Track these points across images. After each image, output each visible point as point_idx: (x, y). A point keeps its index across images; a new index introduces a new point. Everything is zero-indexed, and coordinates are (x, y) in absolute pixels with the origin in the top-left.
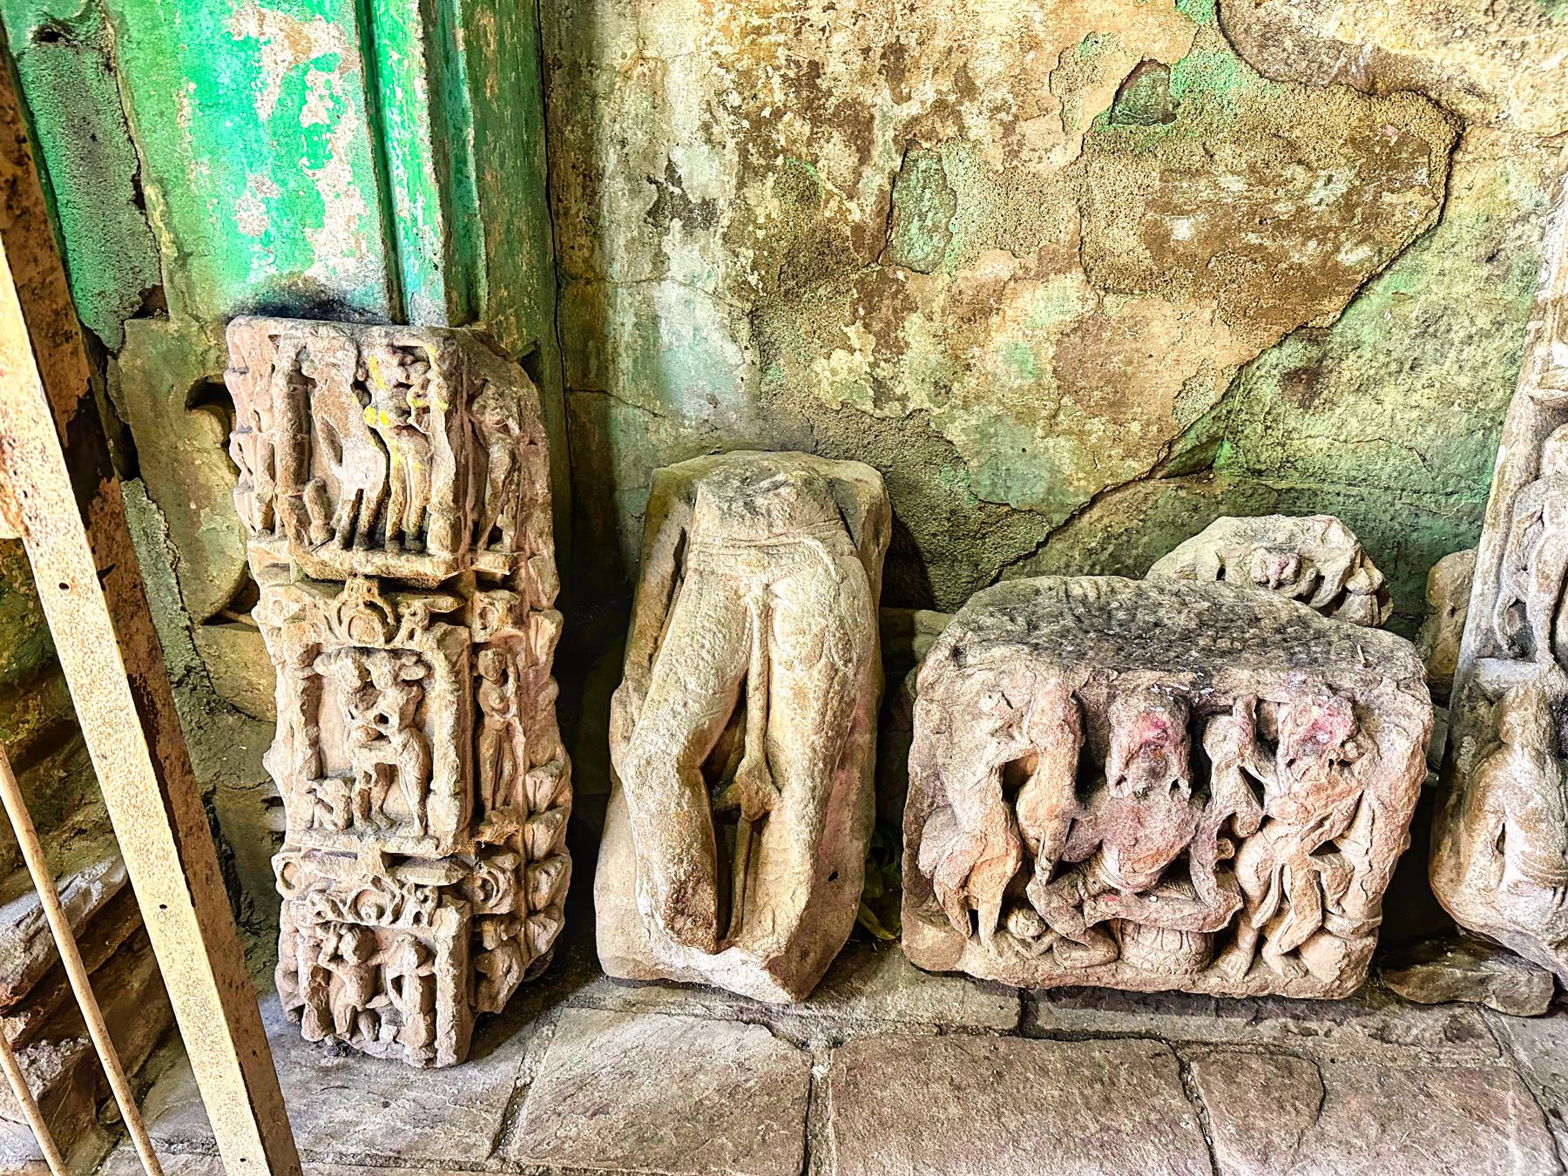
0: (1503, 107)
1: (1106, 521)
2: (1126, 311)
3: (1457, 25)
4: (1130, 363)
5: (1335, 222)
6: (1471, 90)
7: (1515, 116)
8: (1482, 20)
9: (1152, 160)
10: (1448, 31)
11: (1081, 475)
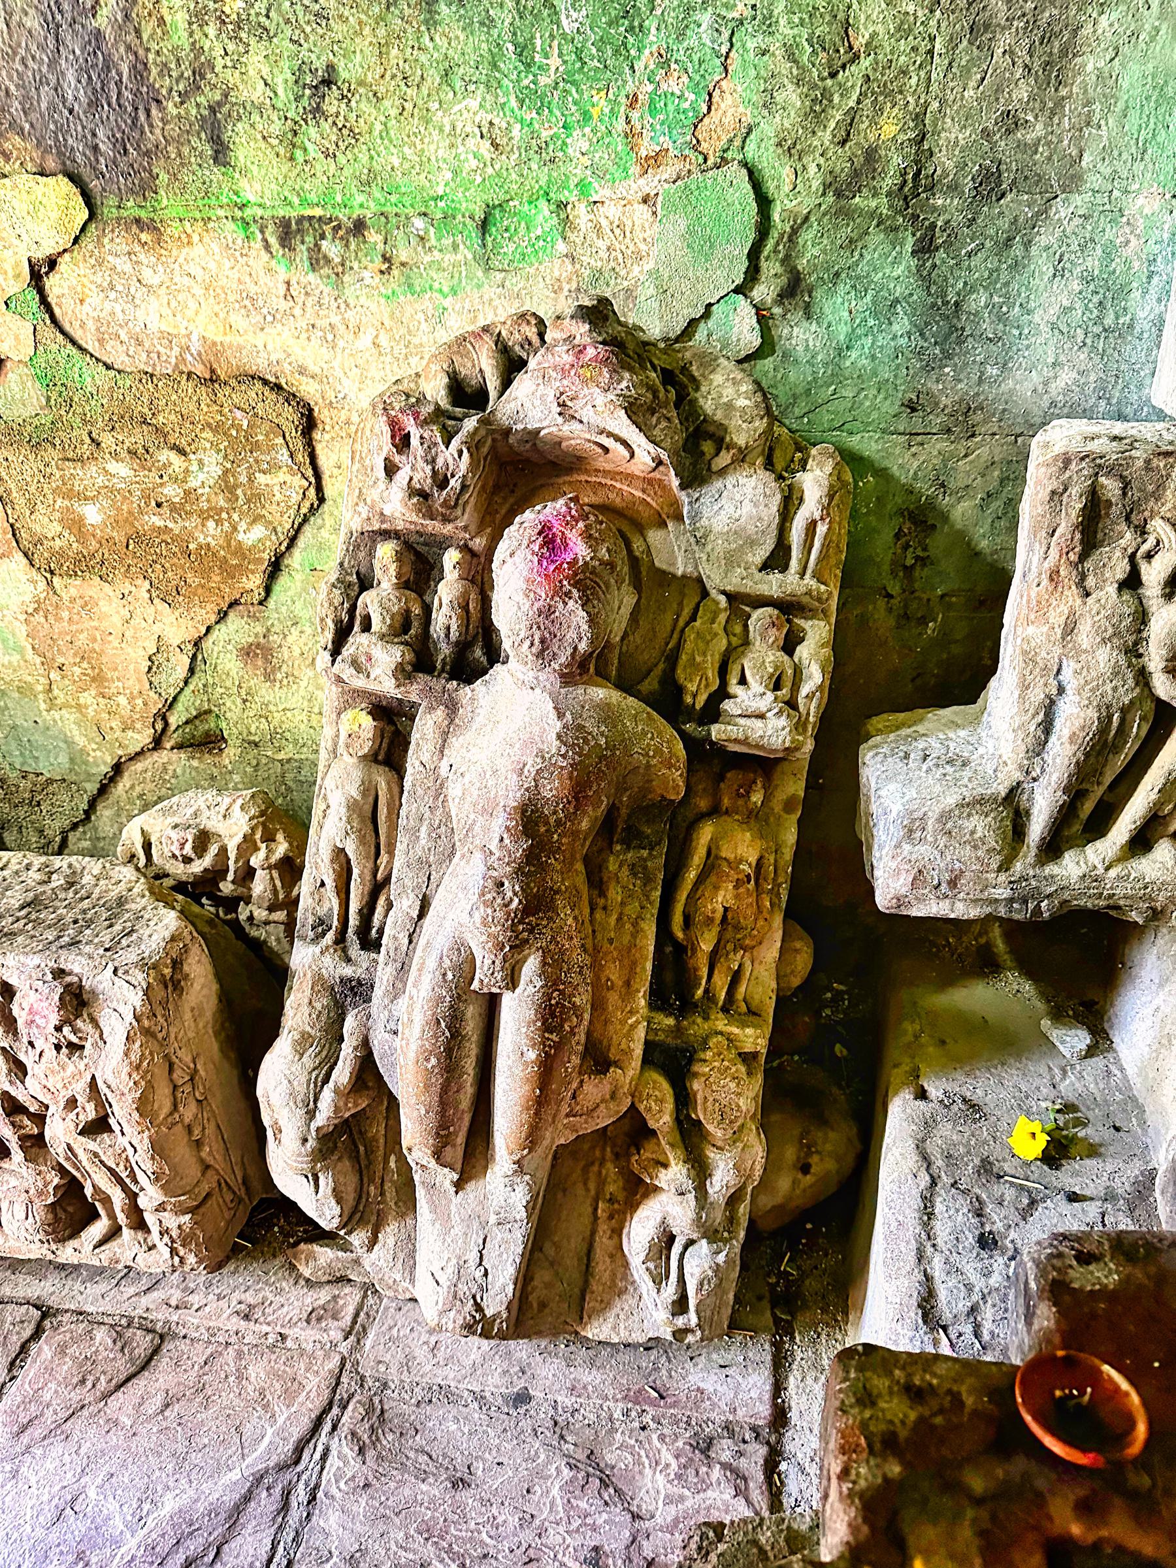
0: (339, 388)
1: (138, 789)
2: (73, 592)
3: (265, 311)
4: (94, 640)
5: (222, 503)
6: (302, 371)
7: (351, 395)
8: (284, 305)
9: (50, 449)
10: (260, 318)
11: (95, 746)
